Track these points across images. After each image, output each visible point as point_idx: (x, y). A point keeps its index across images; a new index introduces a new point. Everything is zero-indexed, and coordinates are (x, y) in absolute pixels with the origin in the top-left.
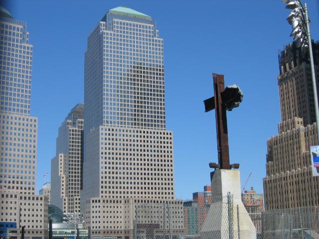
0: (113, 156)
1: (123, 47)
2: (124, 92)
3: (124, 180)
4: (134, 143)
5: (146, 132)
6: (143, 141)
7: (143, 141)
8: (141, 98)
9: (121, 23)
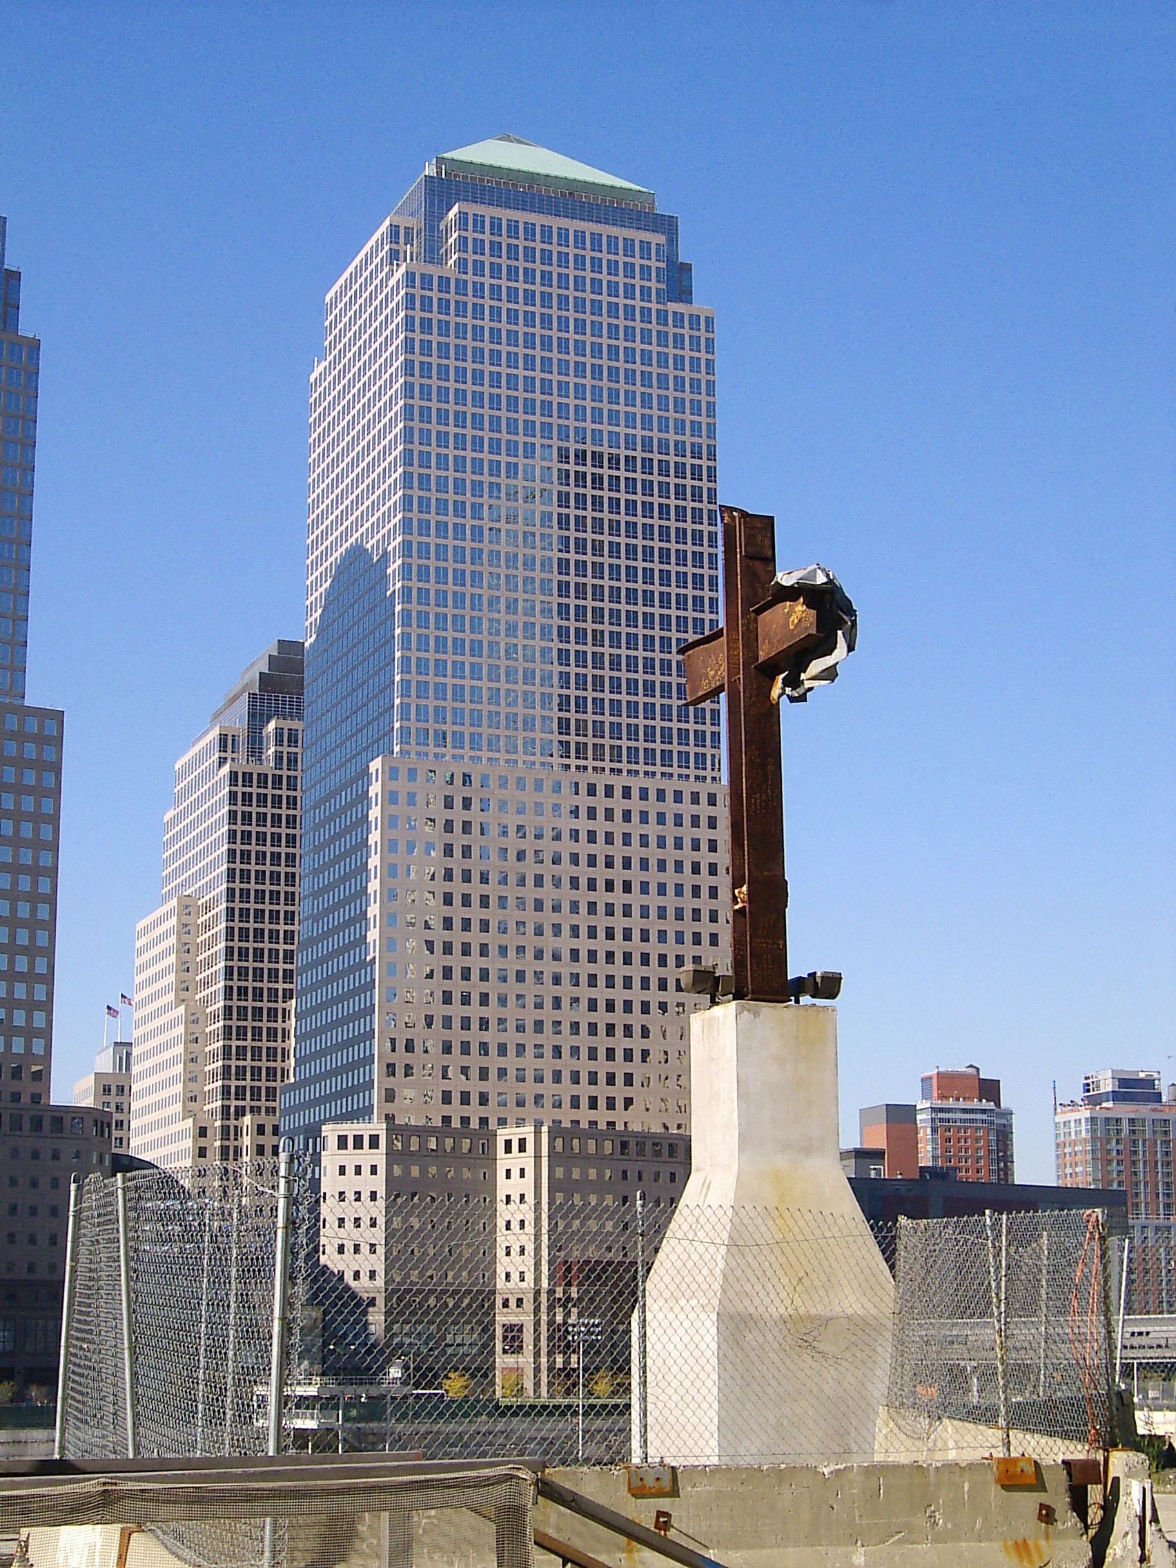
0: (465, 986)
1: (452, 430)
2: (648, 575)
3: (467, 961)
4: (610, 898)
5: (618, 792)
6: (601, 838)
7: (601, 838)
8: (632, 618)
9: (496, 226)
